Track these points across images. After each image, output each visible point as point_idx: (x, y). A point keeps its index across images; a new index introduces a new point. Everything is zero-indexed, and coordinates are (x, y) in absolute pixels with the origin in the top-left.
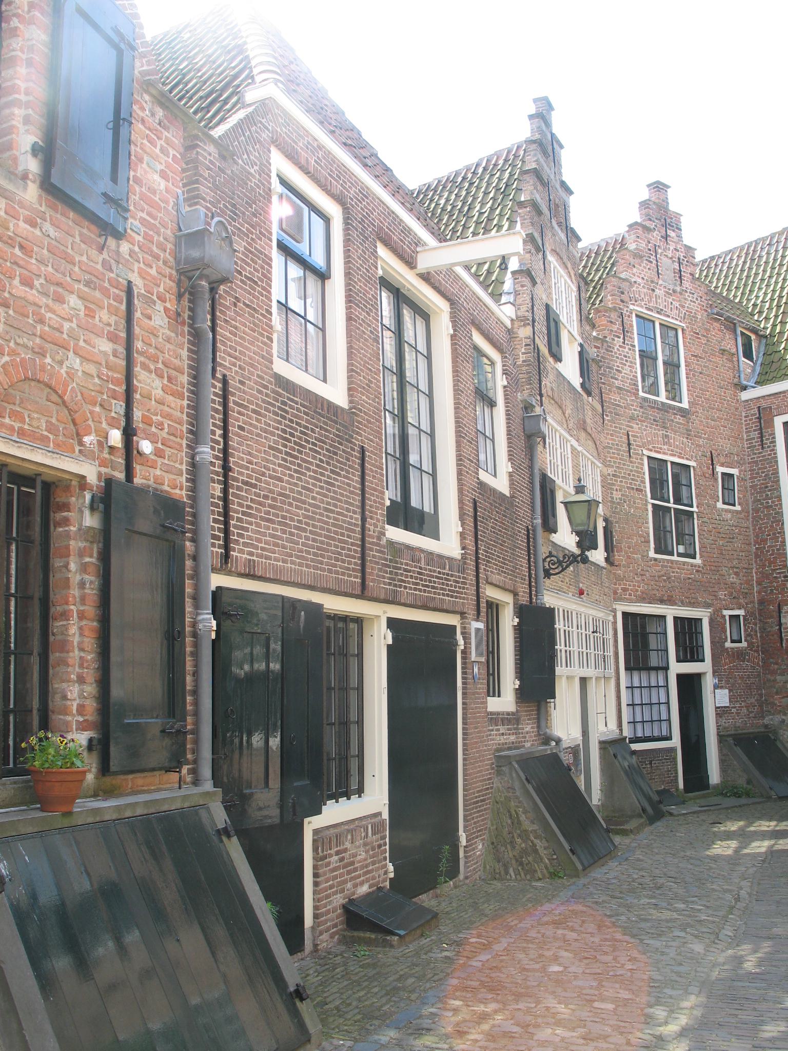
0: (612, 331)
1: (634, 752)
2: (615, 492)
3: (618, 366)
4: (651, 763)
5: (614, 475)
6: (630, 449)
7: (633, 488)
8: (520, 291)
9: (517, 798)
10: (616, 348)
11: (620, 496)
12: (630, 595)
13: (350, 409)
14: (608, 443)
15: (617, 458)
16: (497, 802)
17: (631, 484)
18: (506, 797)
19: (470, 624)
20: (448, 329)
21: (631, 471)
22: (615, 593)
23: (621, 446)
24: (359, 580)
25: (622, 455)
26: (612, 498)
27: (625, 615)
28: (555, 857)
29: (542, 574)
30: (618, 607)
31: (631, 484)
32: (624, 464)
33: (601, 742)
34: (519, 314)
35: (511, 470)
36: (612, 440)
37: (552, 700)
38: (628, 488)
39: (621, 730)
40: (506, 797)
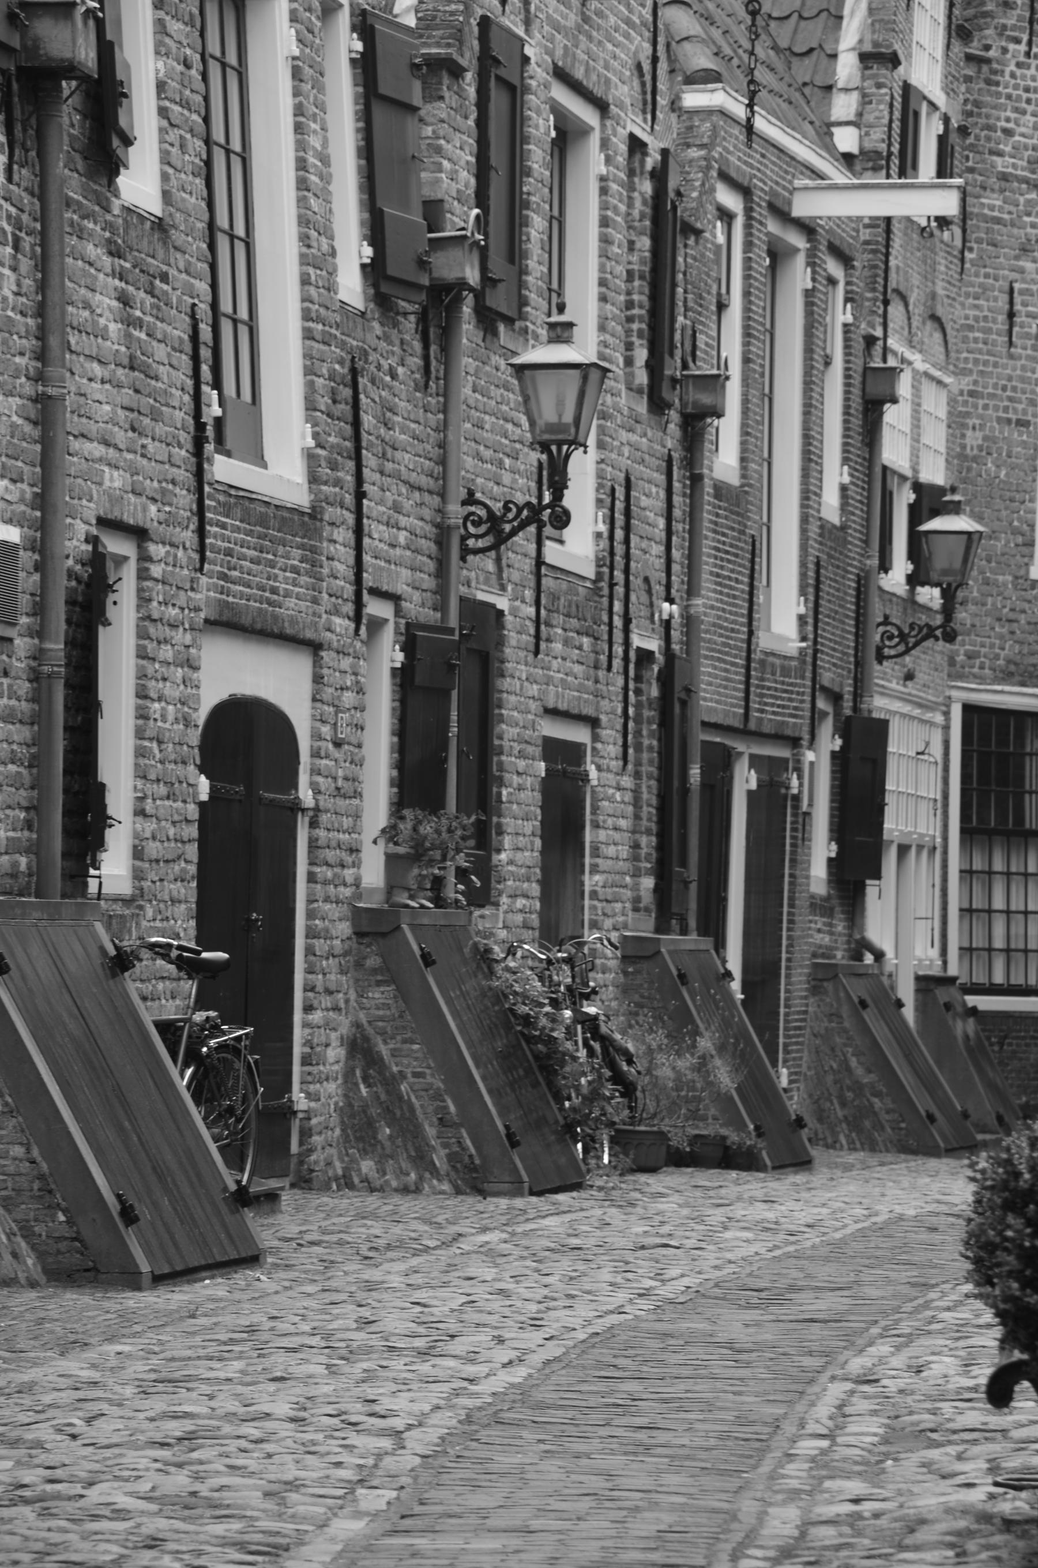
0: (1004, 27)
1: (974, 1011)
2: (969, 433)
3: (1008, 120)
4: (1001, 1044)
5: (972, 394)
6: (1011, 325)
7: (1009, 421)
8: (873, 95)
9: (845, 1031)
10: (1008, 70)
11: (980, 442)
12: (982, 667)
13: (742, 486)
14: (967, 318)
15: (980, 352)
16: (815, 1036)
17: (1006, 409)
18: (826, 1029)
19: (803, 755)
20: (804, 280)
21: (1010, 379)
22: (952, 662)
23: (994, 321)
24: (742, 711)
25: (994, 343)
26: (963, 447)
27: (969, 709)
28: (903, 1125)
29: (872, 653)
30: (954, 694)
31: (1006, 409)
32: (996, 365)
33: (919, 979)
34: (868, 145)
35: (846, 479)
36: (977, 307)
37: (877, 882)
38: (999, 420)
39: (945, 963)
40: (826, 1029)
